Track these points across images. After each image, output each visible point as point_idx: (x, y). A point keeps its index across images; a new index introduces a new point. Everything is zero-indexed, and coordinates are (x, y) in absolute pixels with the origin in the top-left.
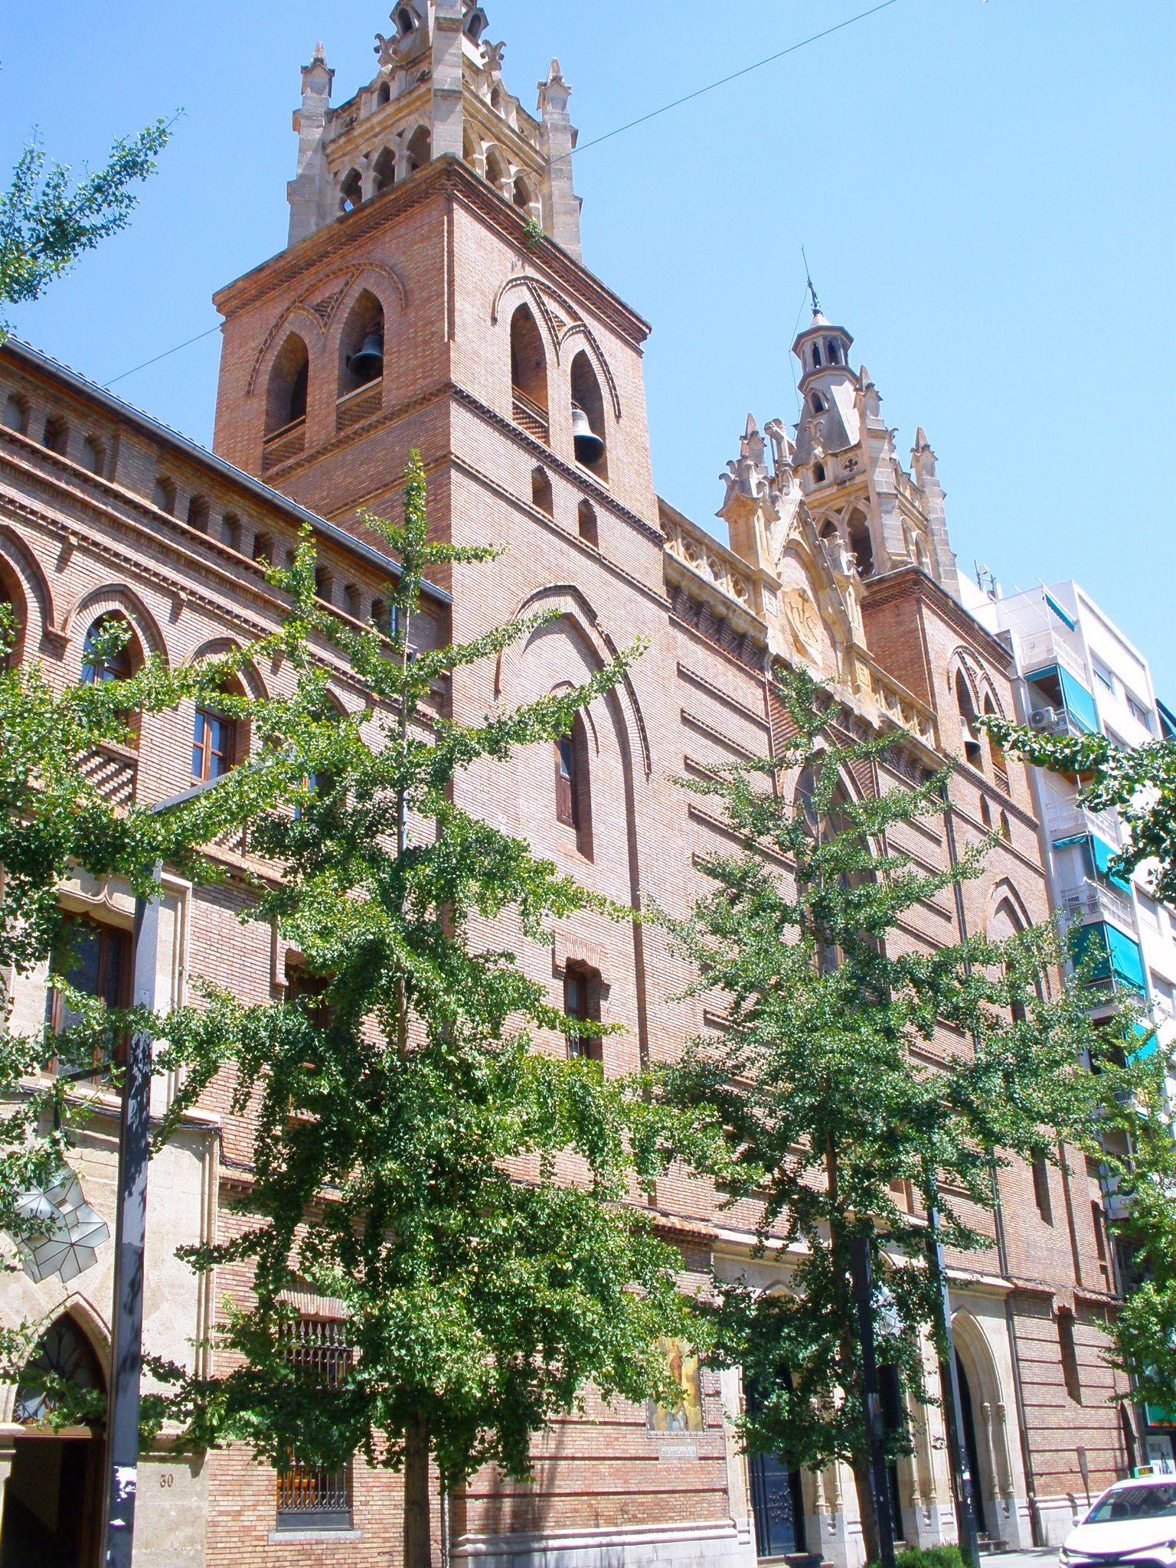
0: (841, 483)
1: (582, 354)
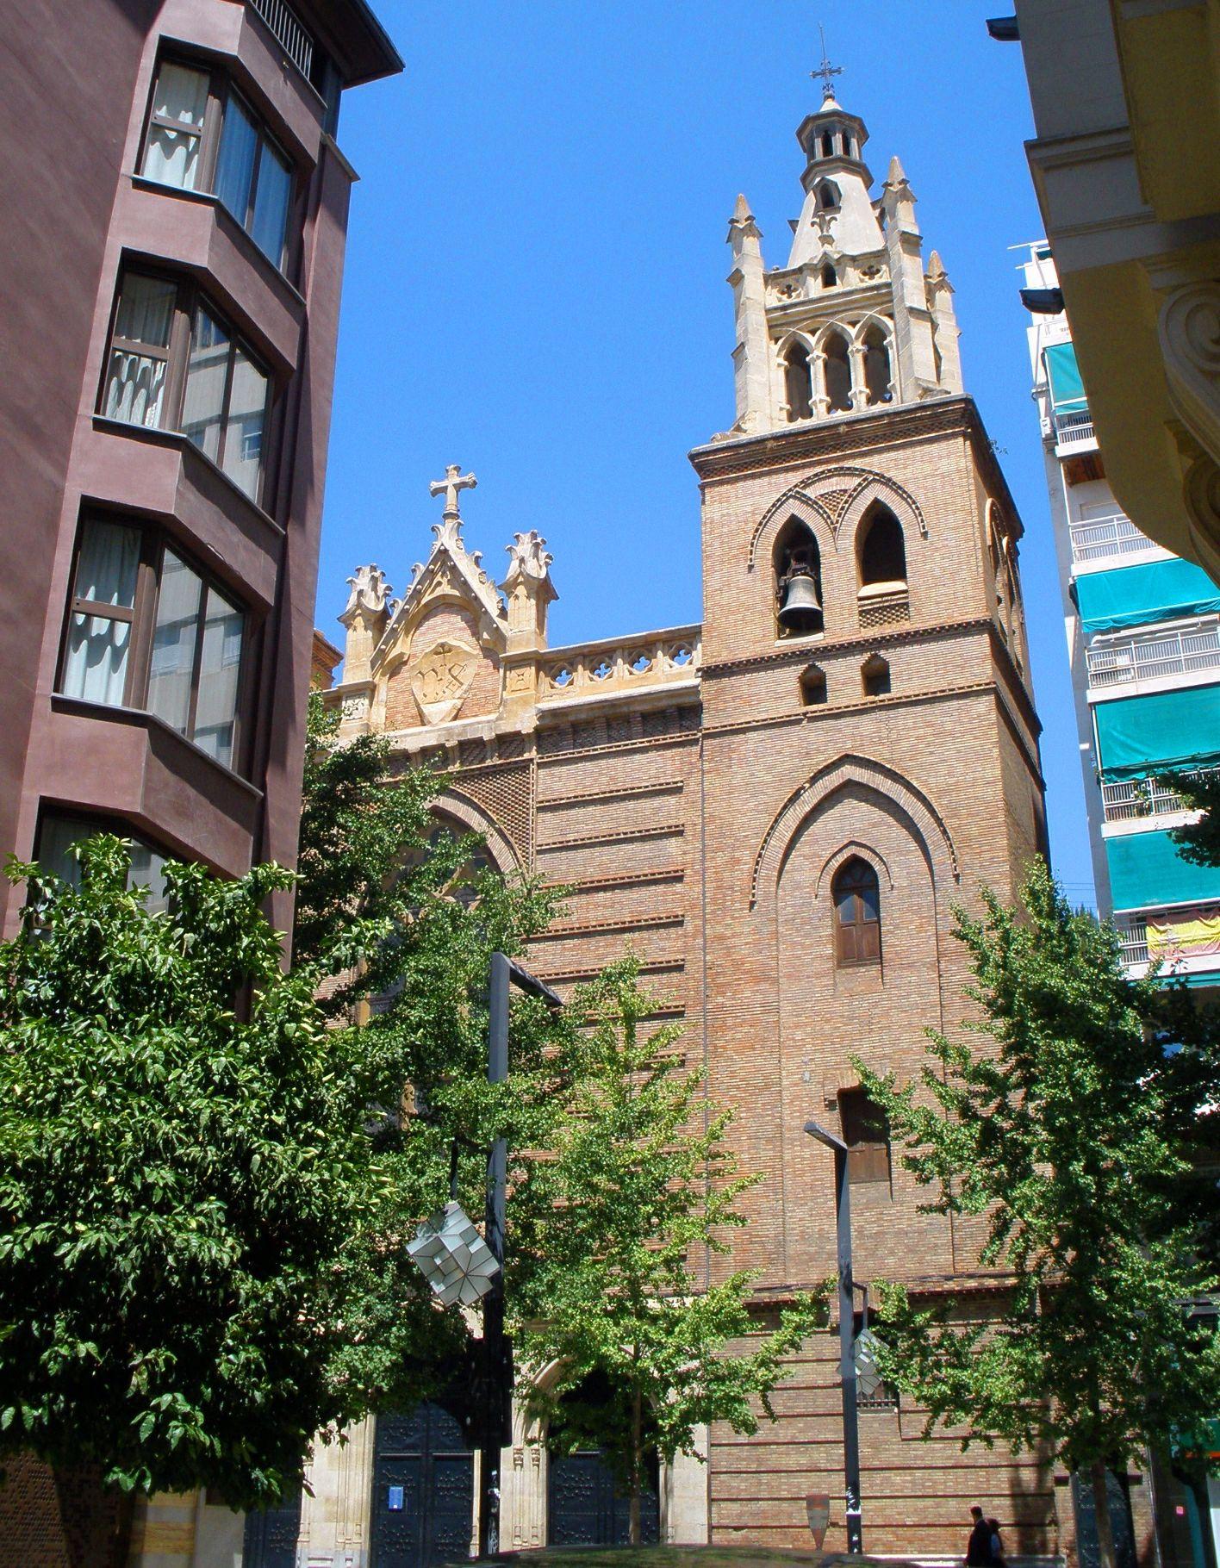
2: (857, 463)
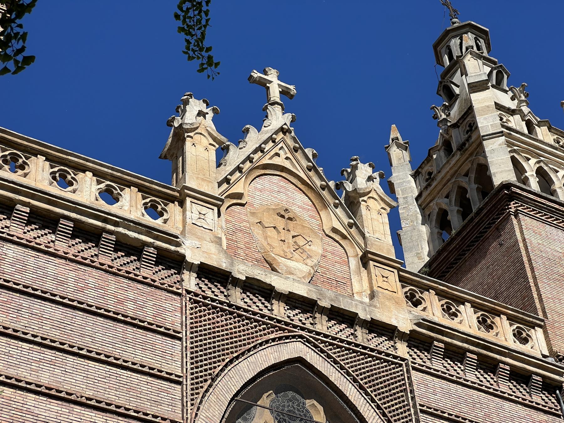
0: (461, 147)
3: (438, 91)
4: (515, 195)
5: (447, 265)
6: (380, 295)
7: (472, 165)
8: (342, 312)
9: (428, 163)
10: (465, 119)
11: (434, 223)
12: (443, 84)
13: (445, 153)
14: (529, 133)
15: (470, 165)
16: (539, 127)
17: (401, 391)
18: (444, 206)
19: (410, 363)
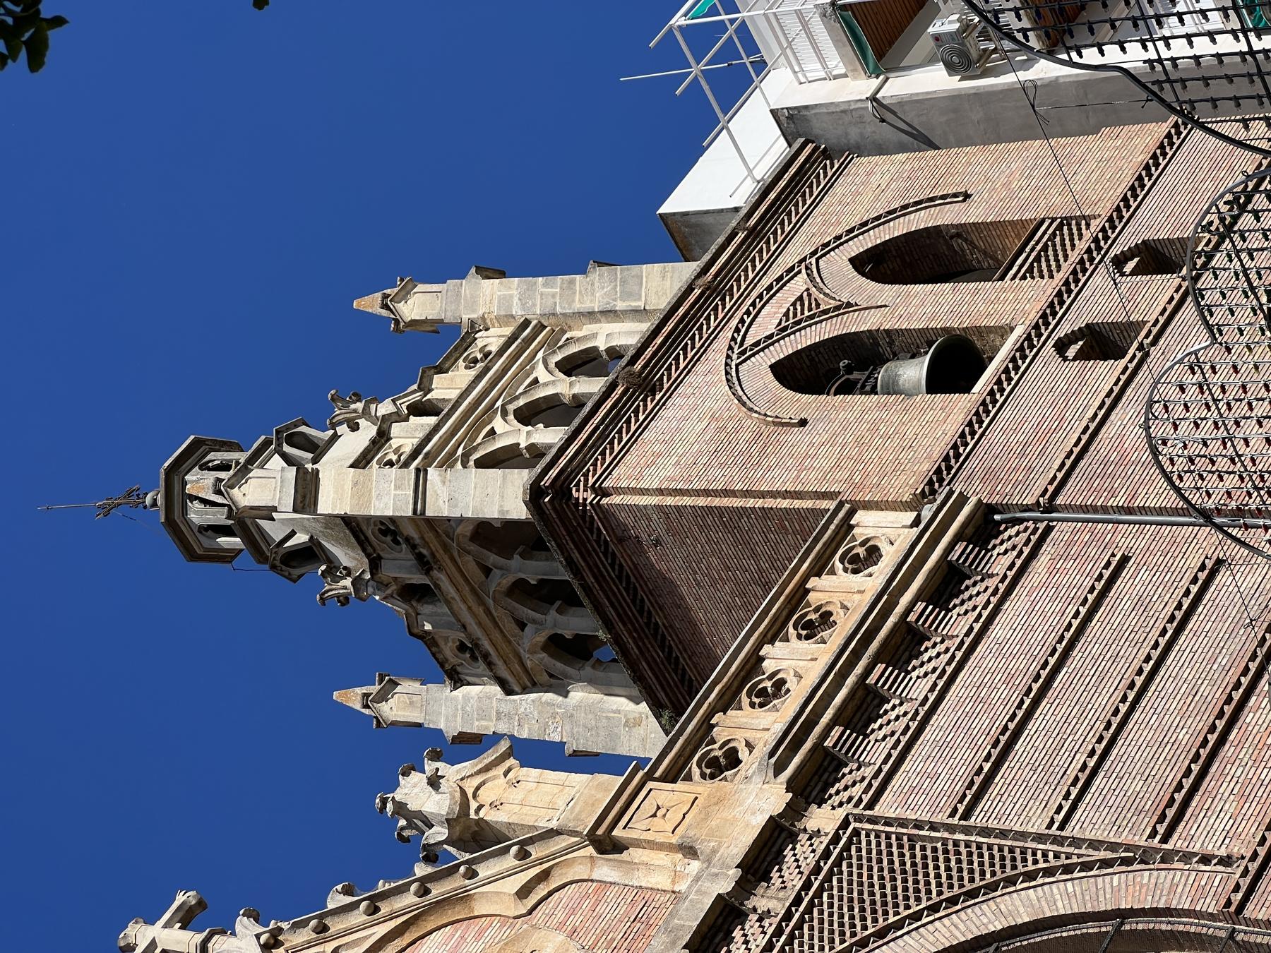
0: (425, 564)
1: (858, 263)
2: (789, 257)
3: (289, 578)
4: (559, 483)
5: (670, 669)
6: (691, 833)
7: (469, 553)
8: (705, 929)
9: (437, 646)
10: (367, 538)
11: (569, 670)
12: (278, 563)
13: (427, 603)
14: (437, 414)
15: (469, 558)
16: (430, 390)
17: (912, 848)
18: (541, 638)
19: (856, 811)
